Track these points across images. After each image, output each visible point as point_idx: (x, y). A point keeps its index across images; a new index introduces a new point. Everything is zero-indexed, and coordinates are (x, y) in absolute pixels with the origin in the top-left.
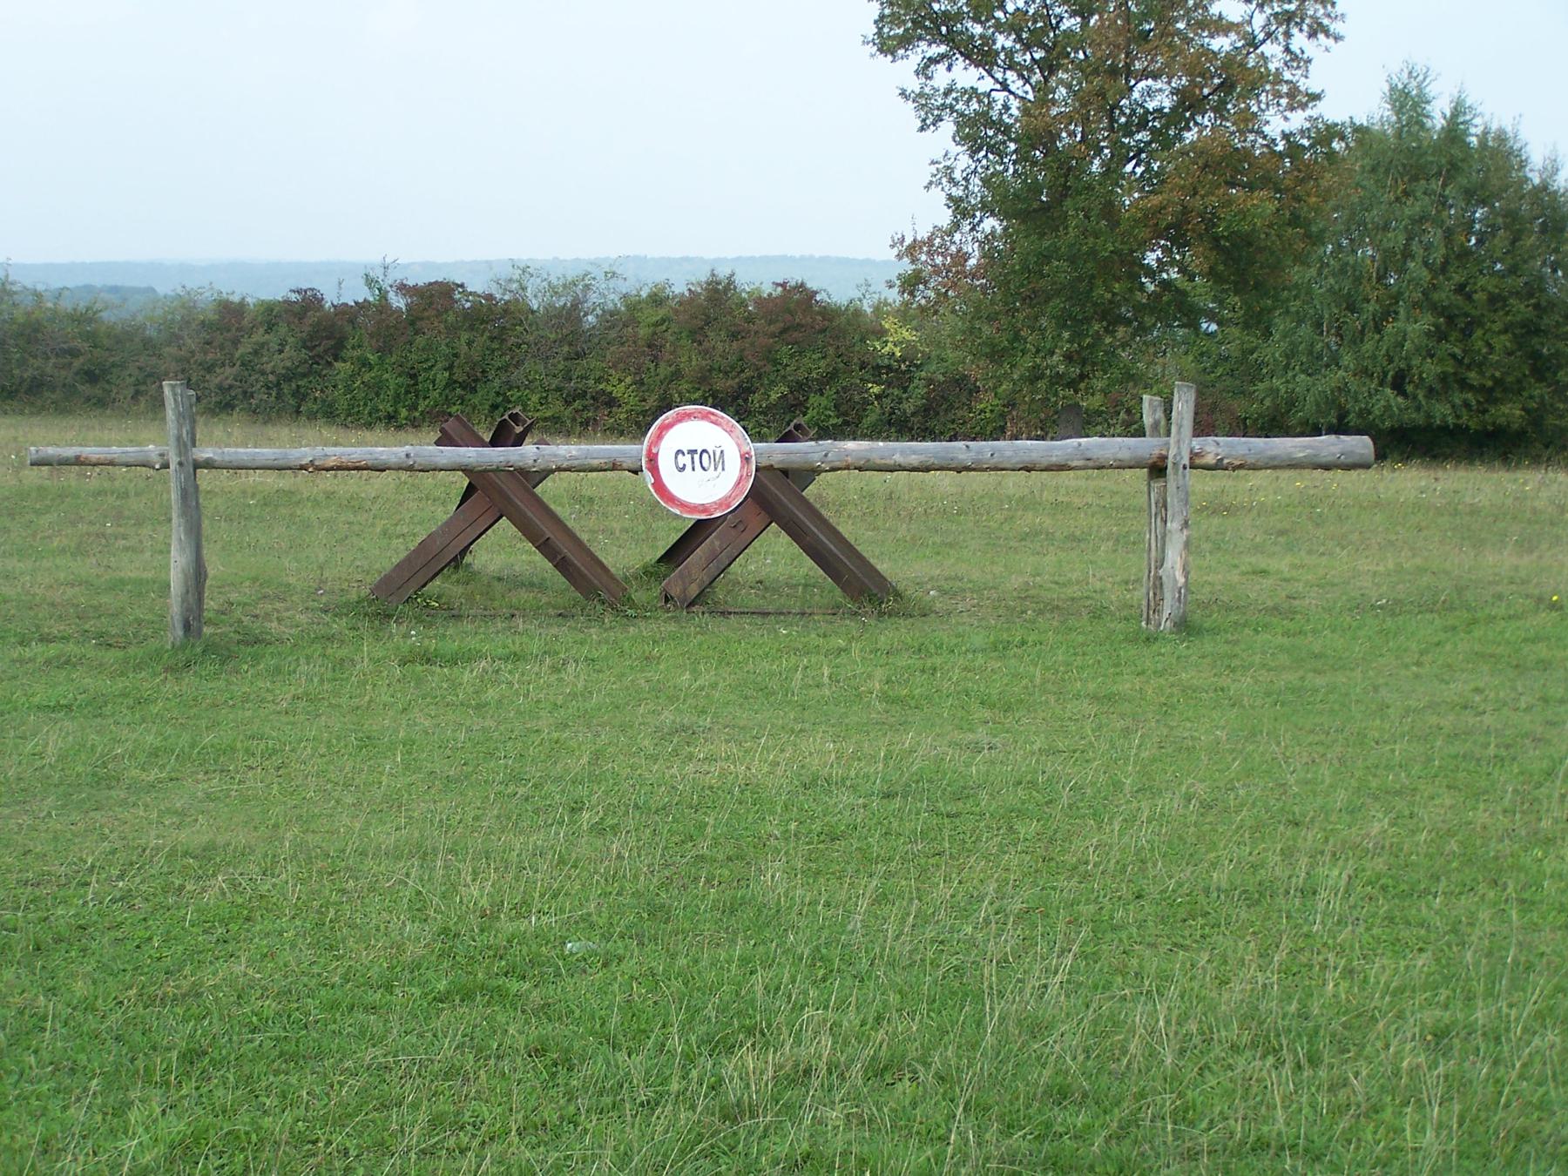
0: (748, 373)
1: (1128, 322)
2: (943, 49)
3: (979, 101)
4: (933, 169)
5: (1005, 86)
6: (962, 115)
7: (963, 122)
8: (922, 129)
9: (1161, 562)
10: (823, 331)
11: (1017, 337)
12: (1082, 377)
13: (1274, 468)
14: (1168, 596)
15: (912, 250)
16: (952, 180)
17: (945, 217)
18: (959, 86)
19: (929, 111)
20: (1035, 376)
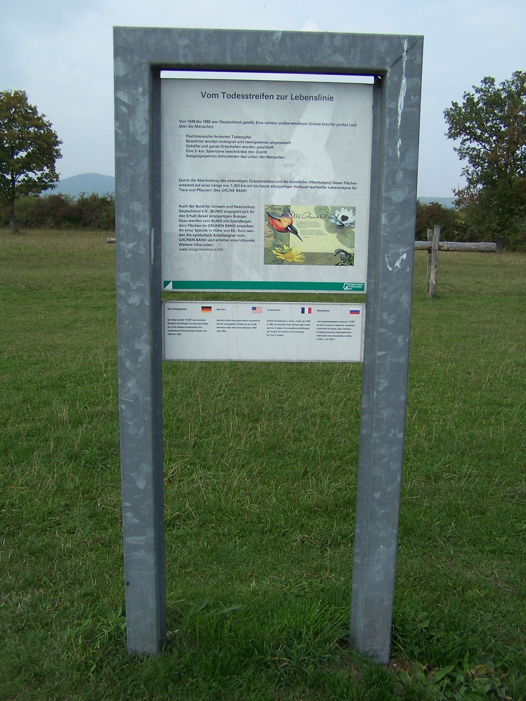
0: (421, 227)
1: (517, 214)
2: (469, 137)
3: (477, 152)
4: (463, 170)
5: (485, 148)
6: (471, 155)
7: (471, 157)
8: (460, 159)
9: (429, 278)
10: (443, 216)
11: (485, 218)
12: (502, 230)
13: (459, 251)
14: (430, 287)
15: (459, 193)
16: (468, 174)
17: (466, 184)
18: (471, 147)
19: (462, 154)
20: (489, 229)
